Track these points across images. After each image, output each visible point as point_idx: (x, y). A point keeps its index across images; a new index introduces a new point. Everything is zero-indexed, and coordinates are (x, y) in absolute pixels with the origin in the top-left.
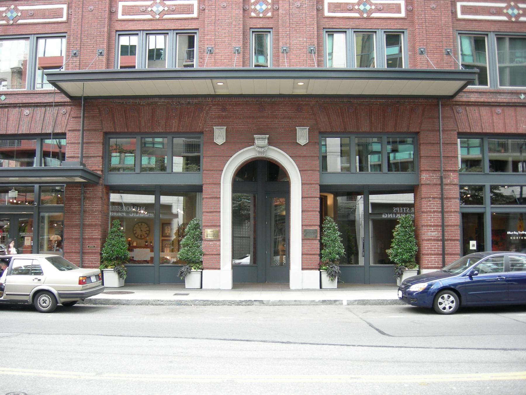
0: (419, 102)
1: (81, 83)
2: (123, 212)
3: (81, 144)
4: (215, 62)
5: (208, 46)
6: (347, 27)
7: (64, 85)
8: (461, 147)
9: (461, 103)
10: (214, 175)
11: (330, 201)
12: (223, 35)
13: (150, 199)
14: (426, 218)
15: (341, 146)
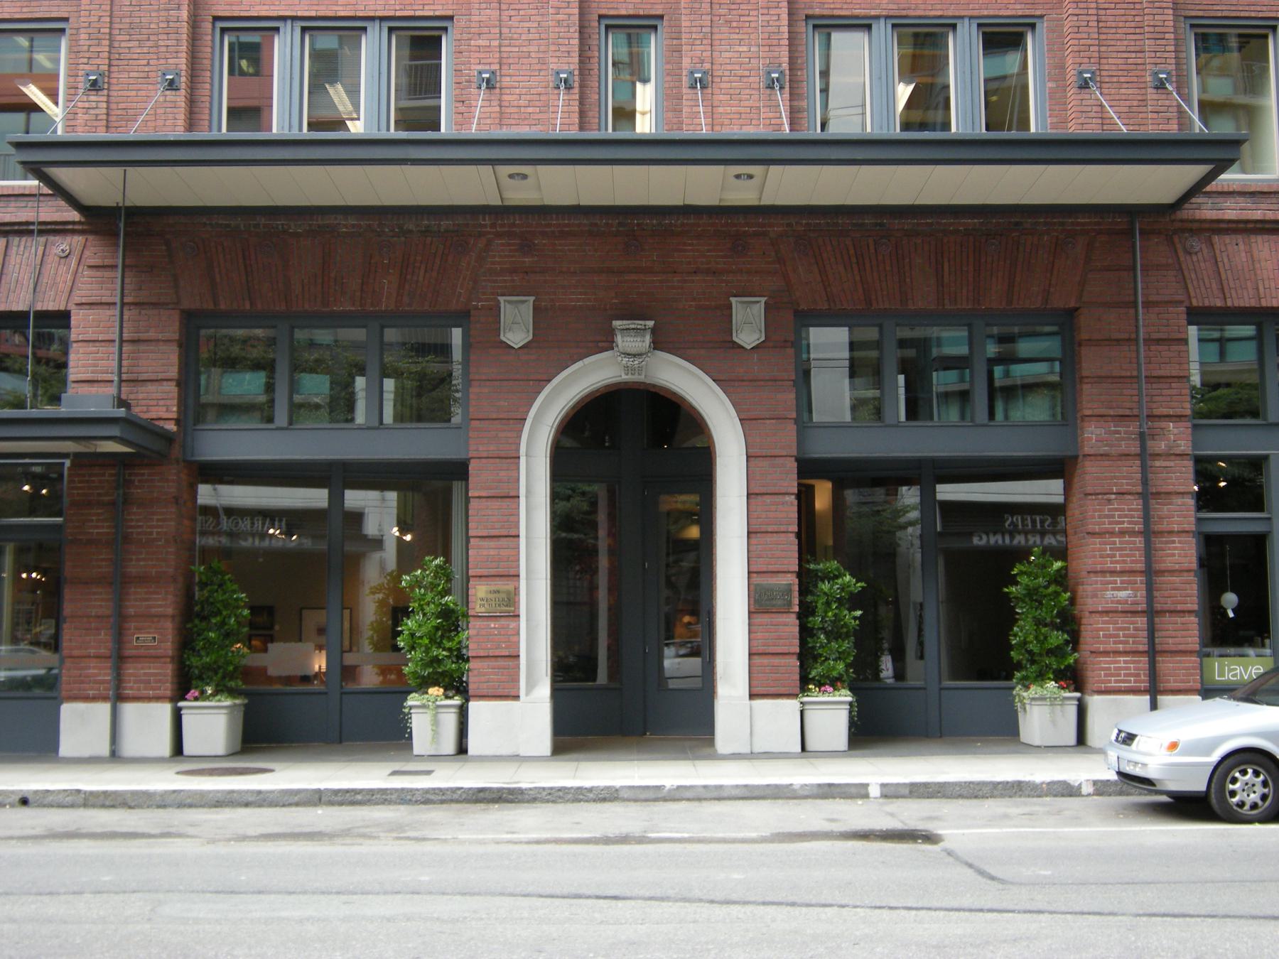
0: (1078, 224)
1: (118, 171)
2: (219, 533)
3: (117, 343)
4: (501, 113)
5: (480, 67)
6: (873, 13)
7: (64, 175)
8: (1200, 340)
9: (1196, 226)
10: (500, 434)
11: (823, 497)
12: (524, 37)
13: (316, 498)
14: (1100, 550)
15: (853, 346)
